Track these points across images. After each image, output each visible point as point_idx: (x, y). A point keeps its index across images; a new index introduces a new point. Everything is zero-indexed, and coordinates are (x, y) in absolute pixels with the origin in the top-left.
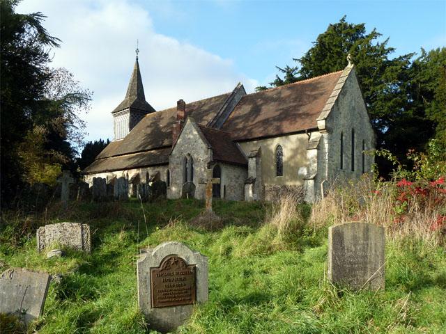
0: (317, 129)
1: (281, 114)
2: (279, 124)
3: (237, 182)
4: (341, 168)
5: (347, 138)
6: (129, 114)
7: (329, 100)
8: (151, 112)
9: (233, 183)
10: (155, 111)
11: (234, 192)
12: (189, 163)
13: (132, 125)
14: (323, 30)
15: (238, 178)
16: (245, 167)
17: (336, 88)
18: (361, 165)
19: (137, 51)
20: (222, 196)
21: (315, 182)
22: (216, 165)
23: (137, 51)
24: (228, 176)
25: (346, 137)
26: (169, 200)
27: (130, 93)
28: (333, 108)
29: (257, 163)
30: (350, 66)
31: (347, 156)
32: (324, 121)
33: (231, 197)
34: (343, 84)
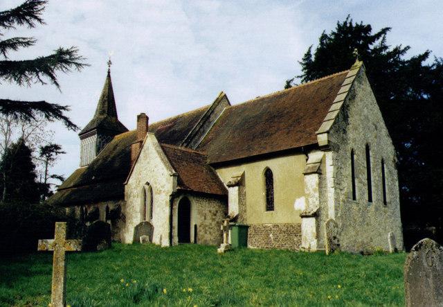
0: (316, 147)
1: (70, 195)
2: (112, 206)
3: (214, 220)
4: (354, 198)
5: (360, 158)
6: (96, 136)
7: (334, 107)
8: (125, 132)
9: (208, 222)
10: (127, 130)
11: (210, 233)
12: (148, 193)
13: (98, 150)
14: (331, 29)
15: (215, 215)
16: (223, 199)
17: (341, 91)
18: (381, 193)
19: (110, 63)
20: (192, 239)
21: (317, 219)
22: (182, 200)
23: (110, 63)
24: (200, 213)
25: (358, 155)
26: (133, 243)
27: (101, 111)
28: (338, 116)
29: (240, 194)
30: (359, 63)
31: (361, 182)
32: (159, 243)
33: (206, 241)
34: (349, 86)
